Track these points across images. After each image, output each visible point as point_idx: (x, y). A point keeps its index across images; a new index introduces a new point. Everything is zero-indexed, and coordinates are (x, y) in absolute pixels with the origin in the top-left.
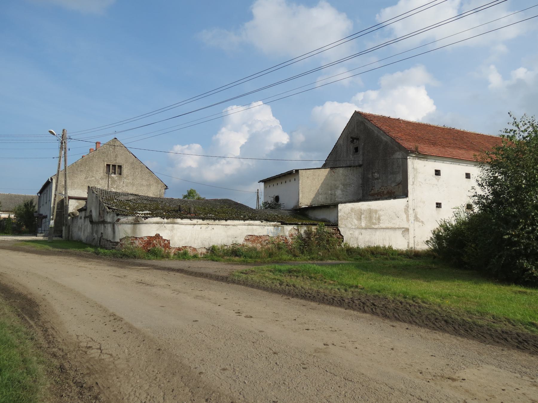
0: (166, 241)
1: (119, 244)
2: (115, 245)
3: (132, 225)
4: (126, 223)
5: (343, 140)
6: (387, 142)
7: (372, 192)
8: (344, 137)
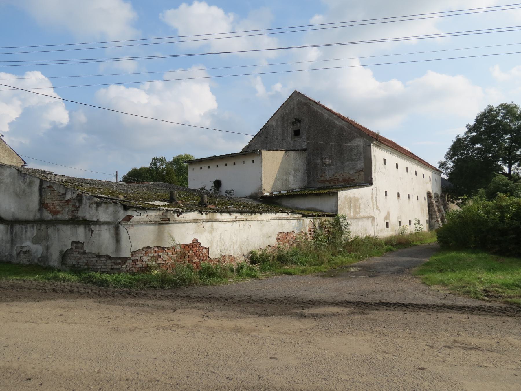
0: (204, 250)
1: (130, 261)
2: (119, 264)
3: (157, 226)
4: (146, 223)
6: (342, 128)
7: (322, 178)
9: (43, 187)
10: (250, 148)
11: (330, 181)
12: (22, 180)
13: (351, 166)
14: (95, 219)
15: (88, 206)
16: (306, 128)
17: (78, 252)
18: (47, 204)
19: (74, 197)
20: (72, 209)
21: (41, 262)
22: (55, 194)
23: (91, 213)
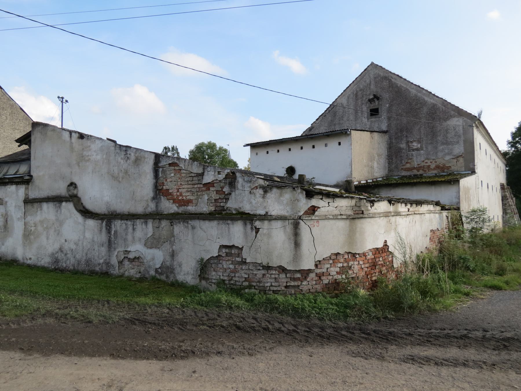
1: (312, 275)
4: (335, 218)
5: (346, 98)
7: (408, 166)
8: (350, 95)
9: (160, 165)
10: (312, 130)
11: (418, 169)
12: (123, 156)
13: (446, 151)
14: (263, 212)
15: (247, 193)
16: (386, 106)
17: (230, 262)
18: (168, 190)
19: (219, 179)
20: (214, 196)
21: (161, 274)
22: (183, 175)
23: (254, 202)
